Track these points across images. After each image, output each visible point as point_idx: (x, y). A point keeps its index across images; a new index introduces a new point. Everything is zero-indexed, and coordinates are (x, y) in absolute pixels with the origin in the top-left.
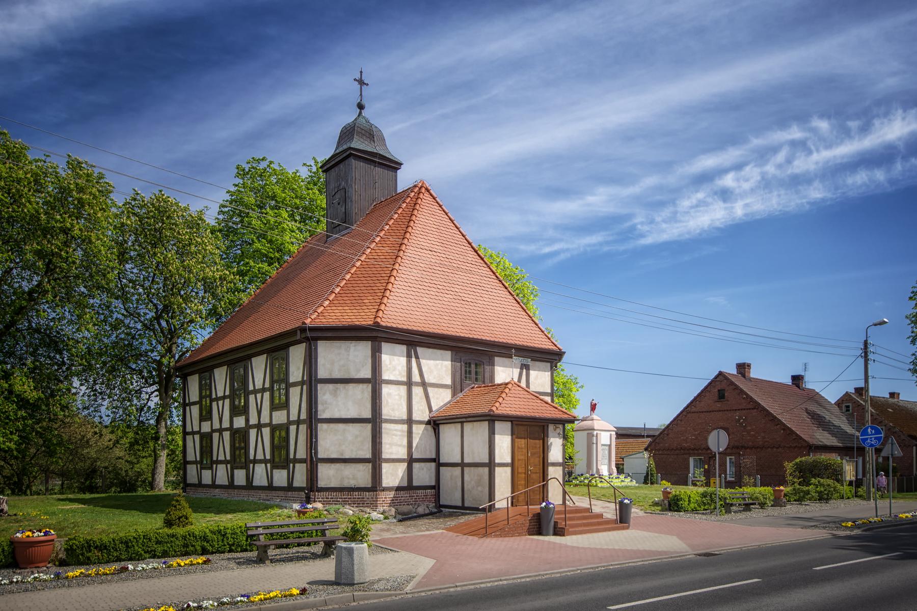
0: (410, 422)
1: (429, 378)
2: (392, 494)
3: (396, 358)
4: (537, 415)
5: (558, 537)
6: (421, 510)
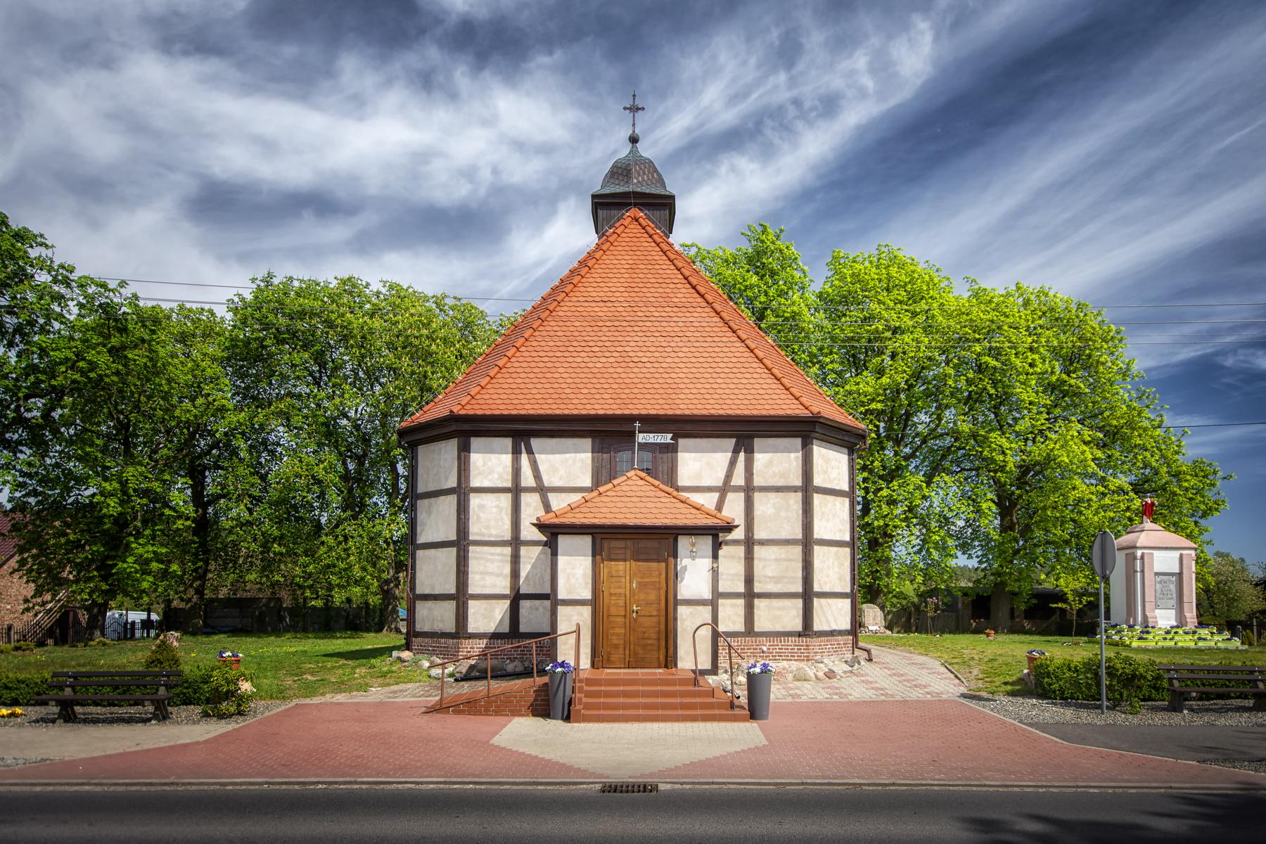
0: (516, 542)
1: (548, 481)
2: (483, 643)
3: (493, 456)
4: (648, 522)
5: (554, 726)
6: (510, 667)
